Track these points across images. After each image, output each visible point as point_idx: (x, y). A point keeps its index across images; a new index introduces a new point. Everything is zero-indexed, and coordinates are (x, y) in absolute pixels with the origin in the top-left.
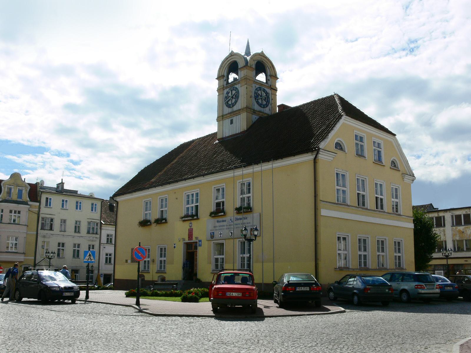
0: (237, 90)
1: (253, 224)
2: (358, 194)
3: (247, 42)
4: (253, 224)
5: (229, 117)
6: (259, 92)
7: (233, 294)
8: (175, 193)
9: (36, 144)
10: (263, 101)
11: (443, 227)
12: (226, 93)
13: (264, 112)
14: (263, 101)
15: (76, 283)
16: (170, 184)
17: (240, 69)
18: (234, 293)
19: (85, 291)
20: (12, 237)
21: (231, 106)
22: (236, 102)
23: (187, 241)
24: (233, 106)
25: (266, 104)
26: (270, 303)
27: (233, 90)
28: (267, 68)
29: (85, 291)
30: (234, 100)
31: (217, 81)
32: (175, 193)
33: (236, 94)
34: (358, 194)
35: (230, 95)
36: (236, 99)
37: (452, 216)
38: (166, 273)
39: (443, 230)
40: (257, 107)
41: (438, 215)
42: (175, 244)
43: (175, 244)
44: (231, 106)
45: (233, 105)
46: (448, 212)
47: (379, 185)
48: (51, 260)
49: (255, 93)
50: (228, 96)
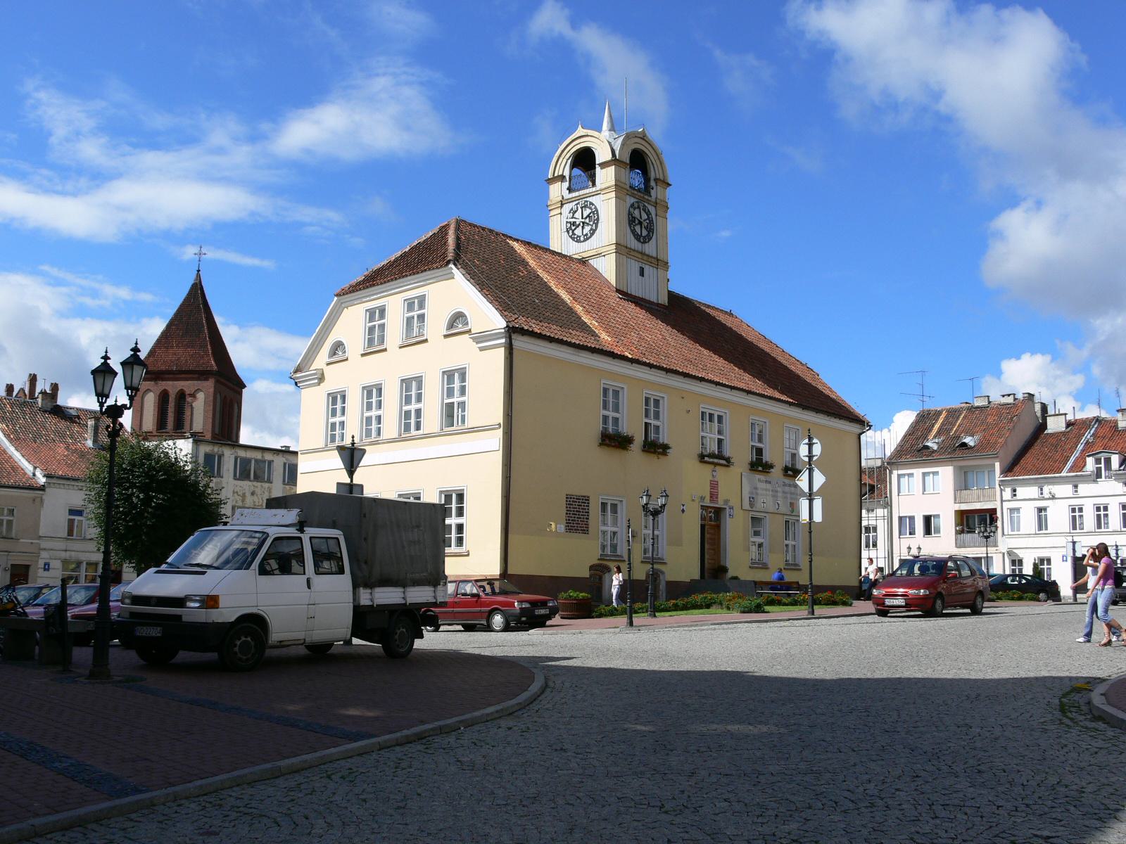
2: (646, 424)
5: (637, 259)
6: (636, 213)
8: (683, 398)
10: (644, 230)
11: (250, 481)
13: (643, 251)
14: (644, 230)
16: (684, 377)
19: (509, 572)
22: (593, 232)
23: (707, 503)
25: (648, 235)
29: (509, 572)
30: (587, 229)
32: (683, 398)
34: (646, 424)
35: (578, 215)
37: (285, 464)
38: (665, 563)
39: (268, 488)
40: (634, 243)
41: (262, 457)
42: (683, 505)
43: (683, 505)
44: (582, 239)
46: (281, 454)
47: (708, 415)
48: (988, 539)
49: (629, 215)
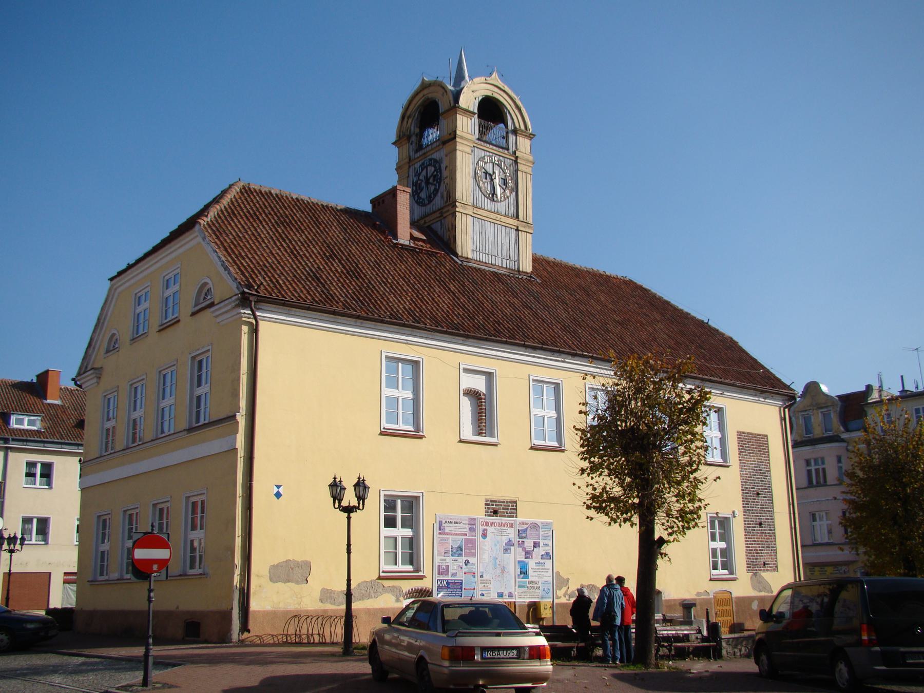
0: (437, 165)
1: (10, 570)
3: (458, 60)
4: (10, 570)
7: (31, 423)
9: (162, 332)
12: (415, 176)
15: (755, 625)
17: (444, 113)
18: (26, 426)
20: (163, 432)
21: (426, 202)
24: (430, 201)
26: (658, 625)
27: (429, 165)
28: (508, 115)
31: (395, 151)
33: (435, 173)
36: (435, 185)
43: (278, 487)
45: (430, 199)
50: (420, 180)
